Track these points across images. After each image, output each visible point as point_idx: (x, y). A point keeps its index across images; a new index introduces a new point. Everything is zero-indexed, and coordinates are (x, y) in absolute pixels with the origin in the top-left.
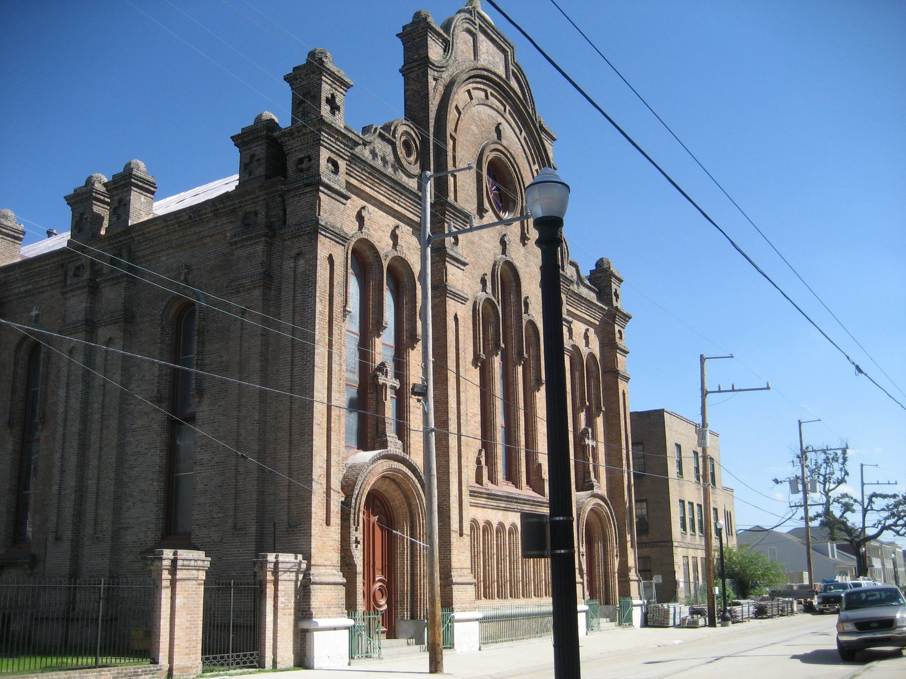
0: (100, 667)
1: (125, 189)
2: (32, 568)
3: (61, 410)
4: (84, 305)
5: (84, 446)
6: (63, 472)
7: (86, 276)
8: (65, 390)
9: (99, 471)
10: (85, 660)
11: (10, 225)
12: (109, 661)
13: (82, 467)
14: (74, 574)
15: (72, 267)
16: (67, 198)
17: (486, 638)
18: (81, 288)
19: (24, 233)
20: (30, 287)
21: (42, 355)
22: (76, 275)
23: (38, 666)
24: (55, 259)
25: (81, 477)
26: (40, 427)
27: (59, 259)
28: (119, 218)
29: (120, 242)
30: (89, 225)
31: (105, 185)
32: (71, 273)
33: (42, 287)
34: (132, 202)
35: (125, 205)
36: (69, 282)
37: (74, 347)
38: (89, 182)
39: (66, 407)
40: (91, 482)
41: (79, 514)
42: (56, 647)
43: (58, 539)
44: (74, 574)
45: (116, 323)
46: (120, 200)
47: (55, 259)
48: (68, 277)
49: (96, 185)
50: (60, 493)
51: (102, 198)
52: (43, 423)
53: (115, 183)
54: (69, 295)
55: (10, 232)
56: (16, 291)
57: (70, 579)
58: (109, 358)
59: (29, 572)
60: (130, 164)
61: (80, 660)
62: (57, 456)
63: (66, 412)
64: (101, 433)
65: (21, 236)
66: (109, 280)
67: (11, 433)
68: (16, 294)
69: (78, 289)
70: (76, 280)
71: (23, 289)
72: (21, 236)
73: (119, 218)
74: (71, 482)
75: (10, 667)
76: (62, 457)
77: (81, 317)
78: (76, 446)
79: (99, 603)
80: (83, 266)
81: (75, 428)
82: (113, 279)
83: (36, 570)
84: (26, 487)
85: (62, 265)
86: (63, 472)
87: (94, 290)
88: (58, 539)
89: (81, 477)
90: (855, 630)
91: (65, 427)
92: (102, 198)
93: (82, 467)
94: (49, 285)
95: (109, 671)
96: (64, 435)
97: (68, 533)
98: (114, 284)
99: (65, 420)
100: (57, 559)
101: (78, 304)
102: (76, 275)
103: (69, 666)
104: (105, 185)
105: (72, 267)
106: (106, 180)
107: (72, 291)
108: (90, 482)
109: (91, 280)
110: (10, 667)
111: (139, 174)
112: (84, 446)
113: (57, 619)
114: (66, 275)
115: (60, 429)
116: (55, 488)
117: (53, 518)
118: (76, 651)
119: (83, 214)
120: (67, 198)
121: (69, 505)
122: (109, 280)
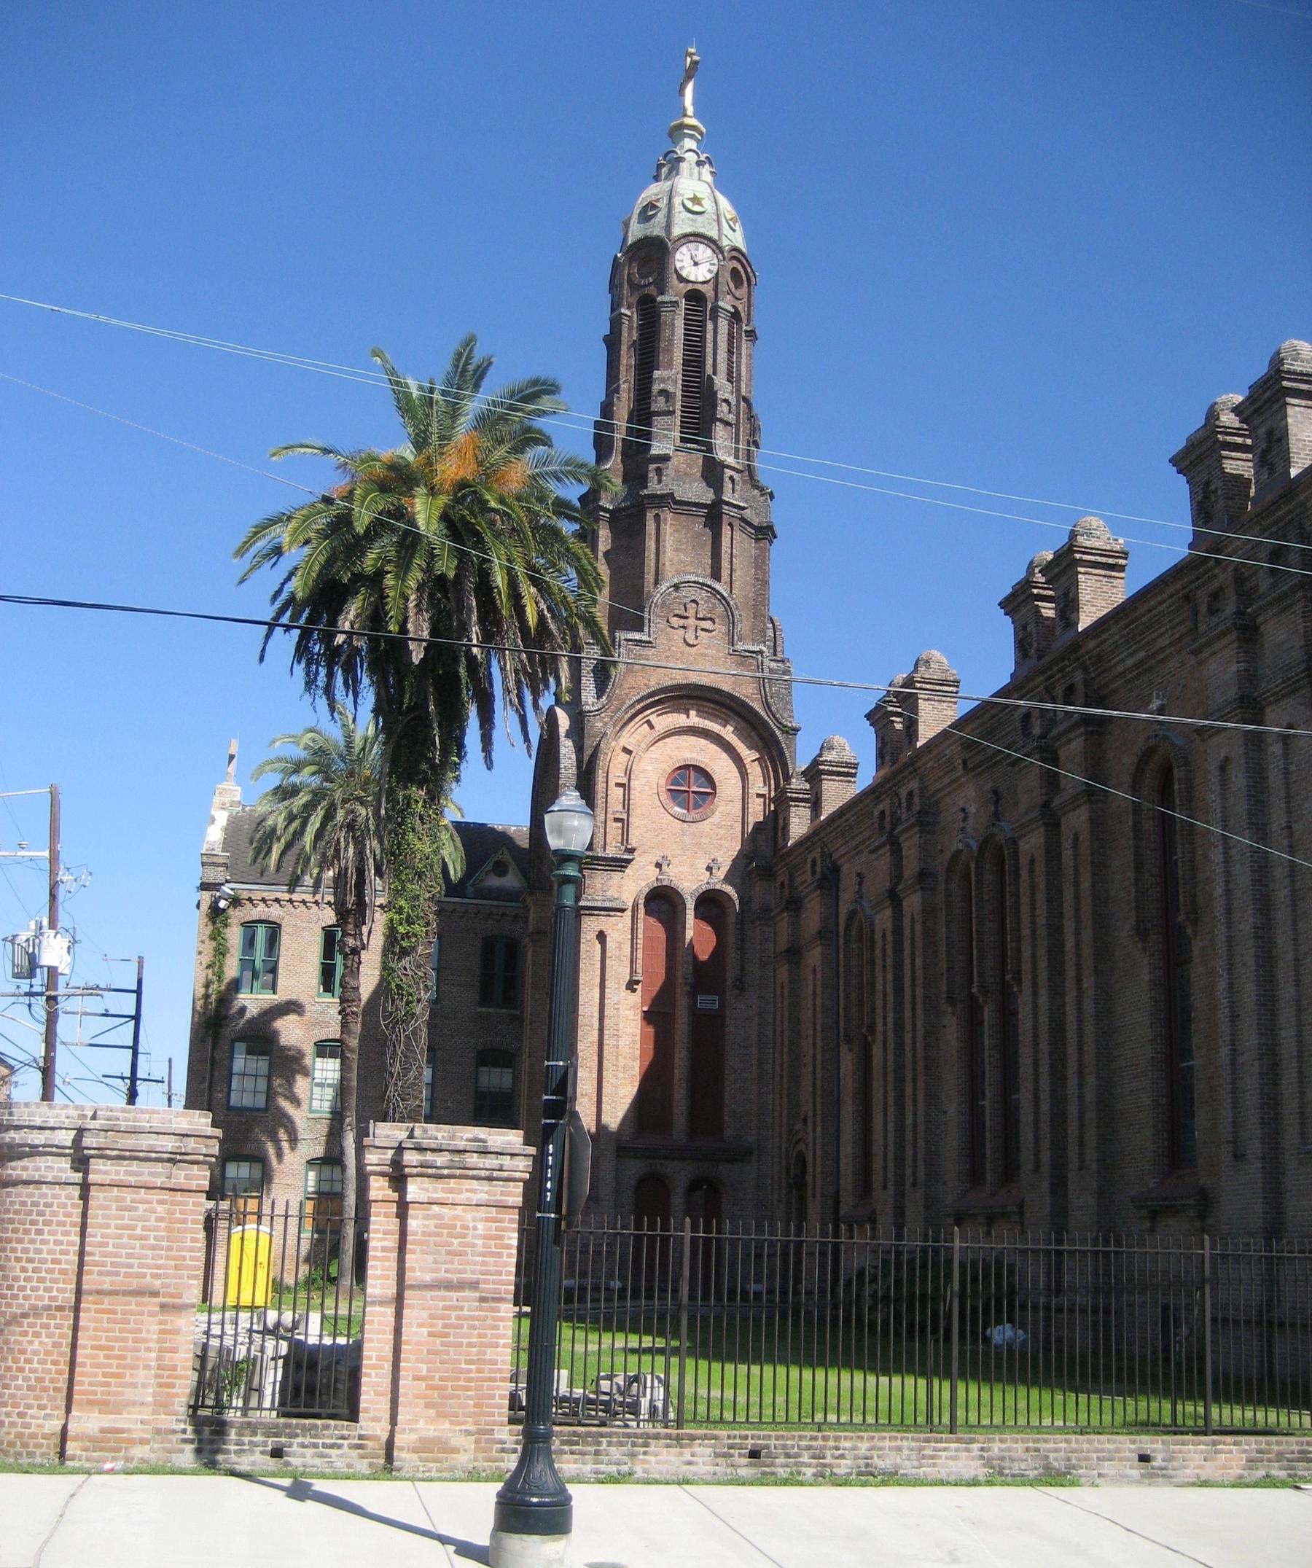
0: (1215, 1433)
1: (1276, 407)
2: (1202, 1216)
3: (1219, 891)
4: (1234, 667)
5: (1267, 959)
6: (1234, 1017)
7: (1230, 608)
8: (1220, 849)
9: (1299, 1009)
10: (1249, 1414)
11: (1097, 544)
12: (1284, 1419)
13: (1268, 1002)
14: (1274, 1230)
15: (1202, 596)
16: (1174, 461)
17: (313, 1365)
18: (1224, 634)
19: (1125, 555)
20: (1141, 655)
21: (1176, 787)
22: (1212, 611)
23: (1119, 1418)
24: (1171, 590)
25: (1269, 1028)
26: (1189, 931)
27: (1178, 586)
28: (1272, 471)
29: (1281, 518)
30: (1221, 502)
31: (1237, 410)
32: (1204, 609)
33: (1161, 650)
34: (1292, 429)
35: (1279, 440)
36: (1202, 627)
37: (1226, 758)
38: (1212, 415)
39: (1227, 882)
40: (1287, 1035)
41: (1271, 1104)
42: (1249, 1381)
43: (1238, 1156)
44: (1274, 1230)
45: (1294, 692)
46: (1270, 433)
47: (1171, 590)
48: (1200, 618)
49: (1223, 418)
50: (1233, 1063)
51: (1239, 440)
52: (1195, 923)
53: (1253, 402)
54: (1204, 655)
55: (1099, 559)
56: (1120, 668)
57: (1268, 1239)
58: (1293, 768)
59: (1198, 1224)
60: (1278, 353)
61: (1226, 1411)
62: (1222, 985)
63: (1228, 892)
64: (1295, 930)
65: (1122, 562)
66: (1269, 605)
67: (1144, 949)
68: (1121, 674)
69: (1218, 637)
70: (1215, 619)
71: (1130, 662)
72: (1122, 562)
73: (1272, 471)
74: (1250, 1039)
75: (1071, 1415)
76: (1231, 986)
77: (1232, 692)
78: (1251, 961)
79: (1202, 1289)
80: (1221, 589)
81: (1246, 924)
82: (1279, 599)
83: (1210, 1221)
84: (1187, 1053)
85: (1187, 598)
86: (1234, 1017)
87: (1248, 633)
88: (1238, 1156)
89: (1269, 1028)
90: (982, 1472)
91: (1229, 925)
92: (1239, 440)
93: (1268, 1002)
94: (1171, 644)
95: (1235, 1444)
96: (1230, 940)
97: (1254, 1146)
98: (1283, 611)
99: (1229, 911)
100: (1239, 1194)
101: (1223, 668)
102: (1212, 611)
103: (1215, 1425)
104: (1237, 410)
105: (1202, 596)
106: (1239, 399)
107: (1209, 644)
108: (1283, 1034)
109: (1240, 613)
110: (1071, 1415)
111: (1298, 367)
112: (1267, 959)
113: (1248, 1322)
114: (1196, 613)
115: (1221, 930)
116: (1224, 1051)
117: (1226, 1114)
118: (1249, 1391)
119: (1208, 484)
120: (1174, 461)
121: (1251, 1084)
122: (1269, 605)
